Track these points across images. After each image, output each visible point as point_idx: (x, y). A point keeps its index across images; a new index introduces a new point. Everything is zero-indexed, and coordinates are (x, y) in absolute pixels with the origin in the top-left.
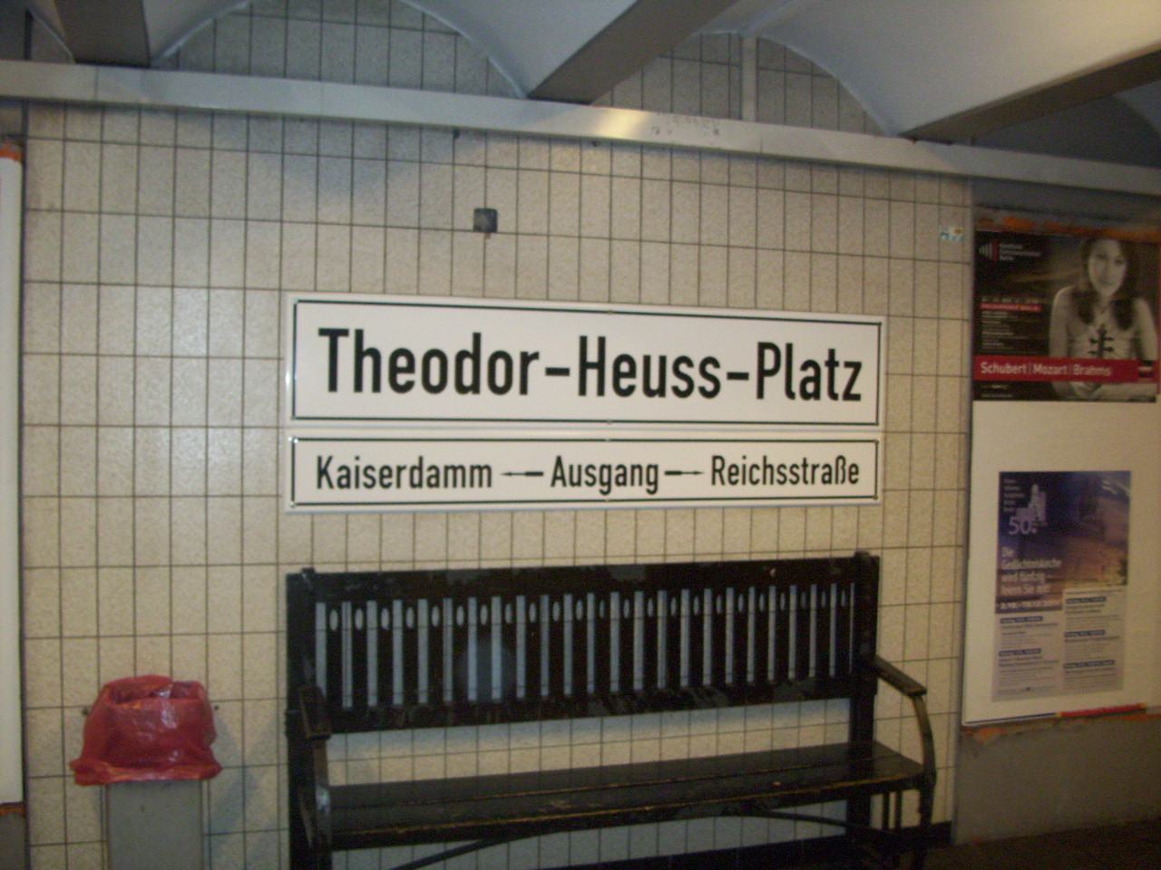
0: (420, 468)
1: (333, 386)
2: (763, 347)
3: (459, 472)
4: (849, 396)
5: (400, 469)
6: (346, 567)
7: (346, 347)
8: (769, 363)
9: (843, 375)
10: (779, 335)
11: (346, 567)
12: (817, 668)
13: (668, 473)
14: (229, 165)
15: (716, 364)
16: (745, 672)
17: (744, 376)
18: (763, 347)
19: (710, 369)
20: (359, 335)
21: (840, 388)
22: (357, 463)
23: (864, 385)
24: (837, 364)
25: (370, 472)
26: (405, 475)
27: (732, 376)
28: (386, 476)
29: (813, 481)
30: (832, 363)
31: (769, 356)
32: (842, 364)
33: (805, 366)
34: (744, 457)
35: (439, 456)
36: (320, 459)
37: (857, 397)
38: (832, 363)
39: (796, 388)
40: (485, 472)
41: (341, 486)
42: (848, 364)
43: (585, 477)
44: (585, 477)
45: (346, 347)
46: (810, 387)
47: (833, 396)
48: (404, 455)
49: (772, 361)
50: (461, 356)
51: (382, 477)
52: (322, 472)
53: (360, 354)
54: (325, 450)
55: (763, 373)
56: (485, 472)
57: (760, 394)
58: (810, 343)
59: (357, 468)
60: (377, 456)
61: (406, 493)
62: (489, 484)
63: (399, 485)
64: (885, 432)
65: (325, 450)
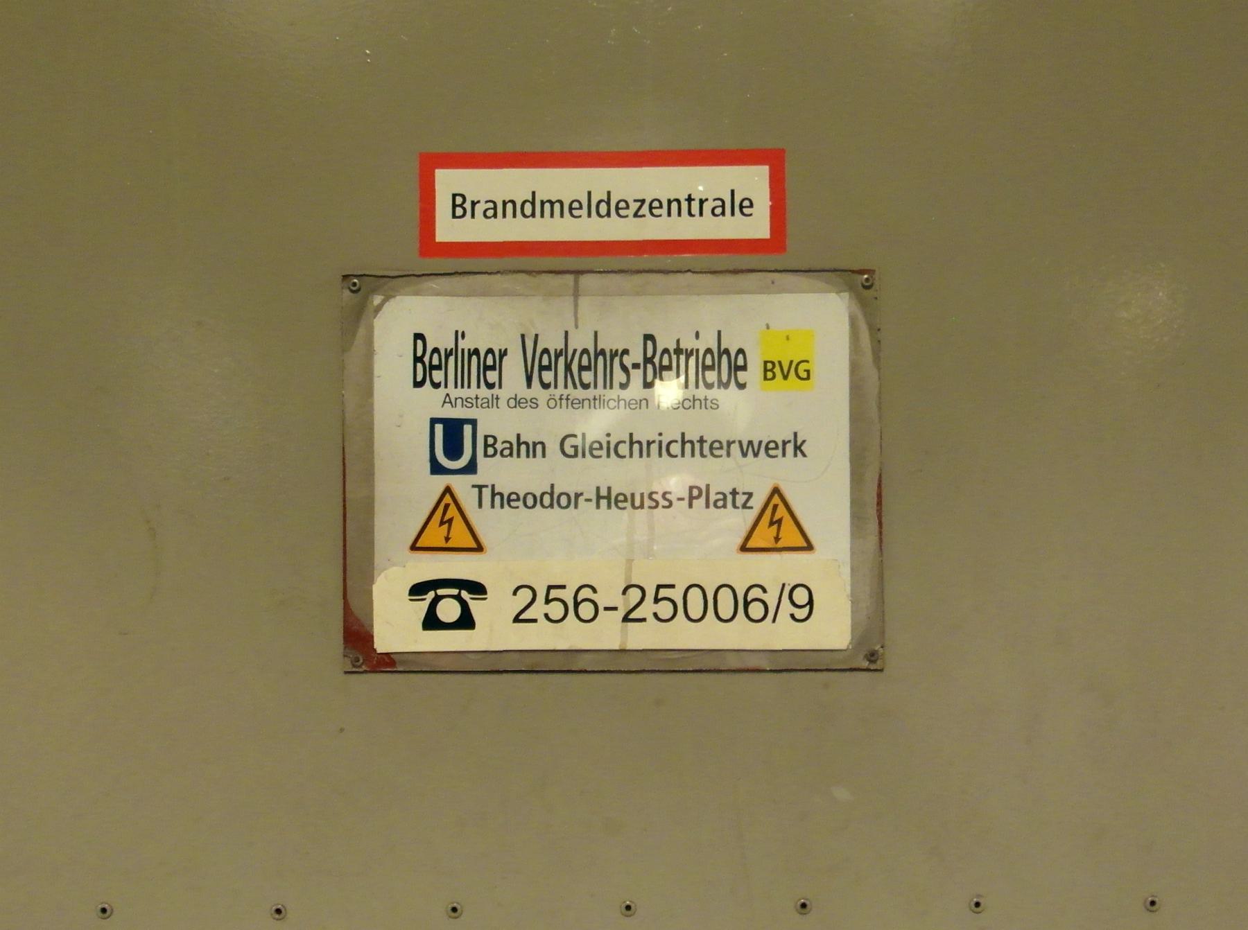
1: (480, 505)
7: (487, 493)
13: (606, 609)
20: (493, 486)
29: (701, 214)
43: (647, 503)
44: (647, 503)
45: (487, 493)
49: (694, 495)
50: (543, 494)
53: (493, 495)
55: (691, 498)
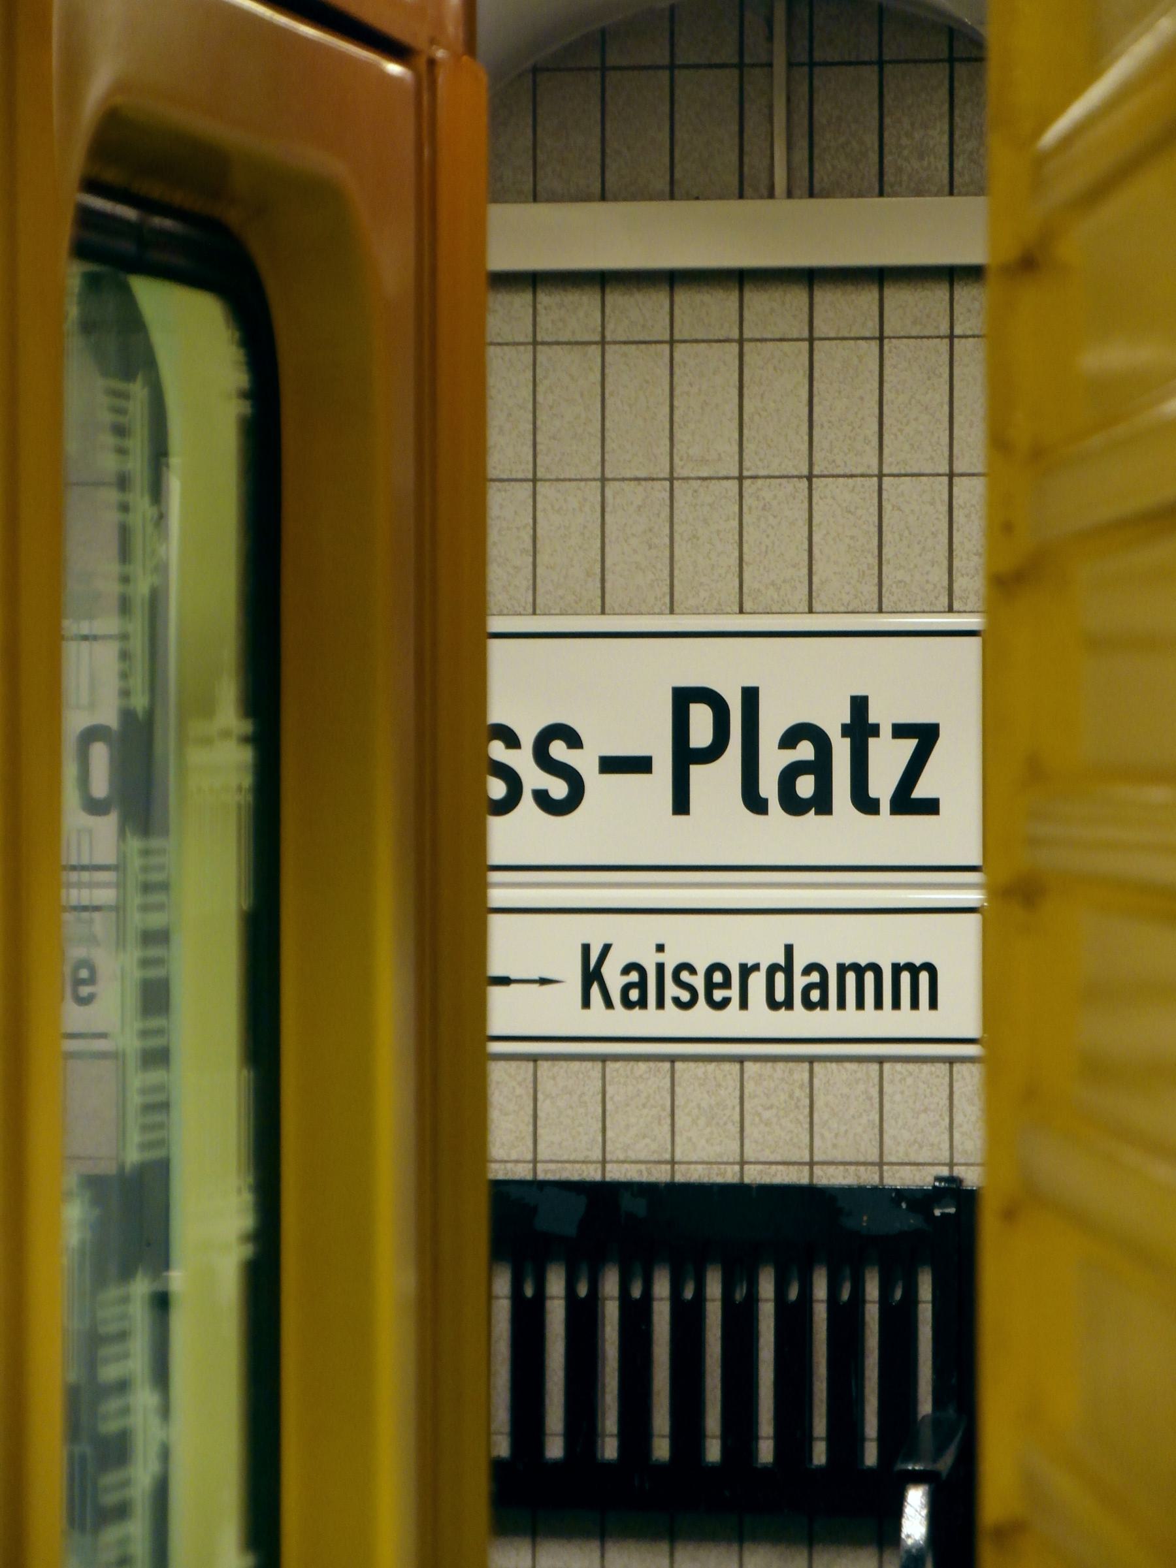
0: (788, 970)
2: (683, 698)
3: (869, 977)
4: (906, 802)
5: (746, 971)
6: (951, 1170)
8: (701, 733)
9: (888, 759)
10: (724, 670)
11: (951, 1170)
12: (831, 1439)
14: (637, 376)
15: (573, 740)
16: (808, 1439)
17: (642, 765)
18: (683, 698)
19: (558, 750)
21: (882, 786)
22: (660, 957)
23: (955, 774)
24: (875, 731)
25: (685, 976)
26: (757, 982)
27: (610, 765)
28: (719, 984)
30: (860, 728)
31: (701, 718)
32: (886, 731)
33: (790, 739)
34: (660, 948)
35: (827, 944)
36: (586, 949)
37: (930, 807)
38: (860, 728)
39: (769, 788)
40: (924, 977)
41: (628, 1004)
42: (900, 731)
46: (805, 786)
47: (865, 804)
48: (756, 942)
49: (706, 730)
51: (710, 986)
52: (592, 976)
54: (596, 931)
55: (685, 757)
56: (924, 977)
57: (681, 804)
58: (803, 687)
59: (660, 967)
60: (700, 944)
61: (758, 1019)
62: (933, 1004)
63: (744, 1005)
64: (1017, 895)
65: (596, 931)
